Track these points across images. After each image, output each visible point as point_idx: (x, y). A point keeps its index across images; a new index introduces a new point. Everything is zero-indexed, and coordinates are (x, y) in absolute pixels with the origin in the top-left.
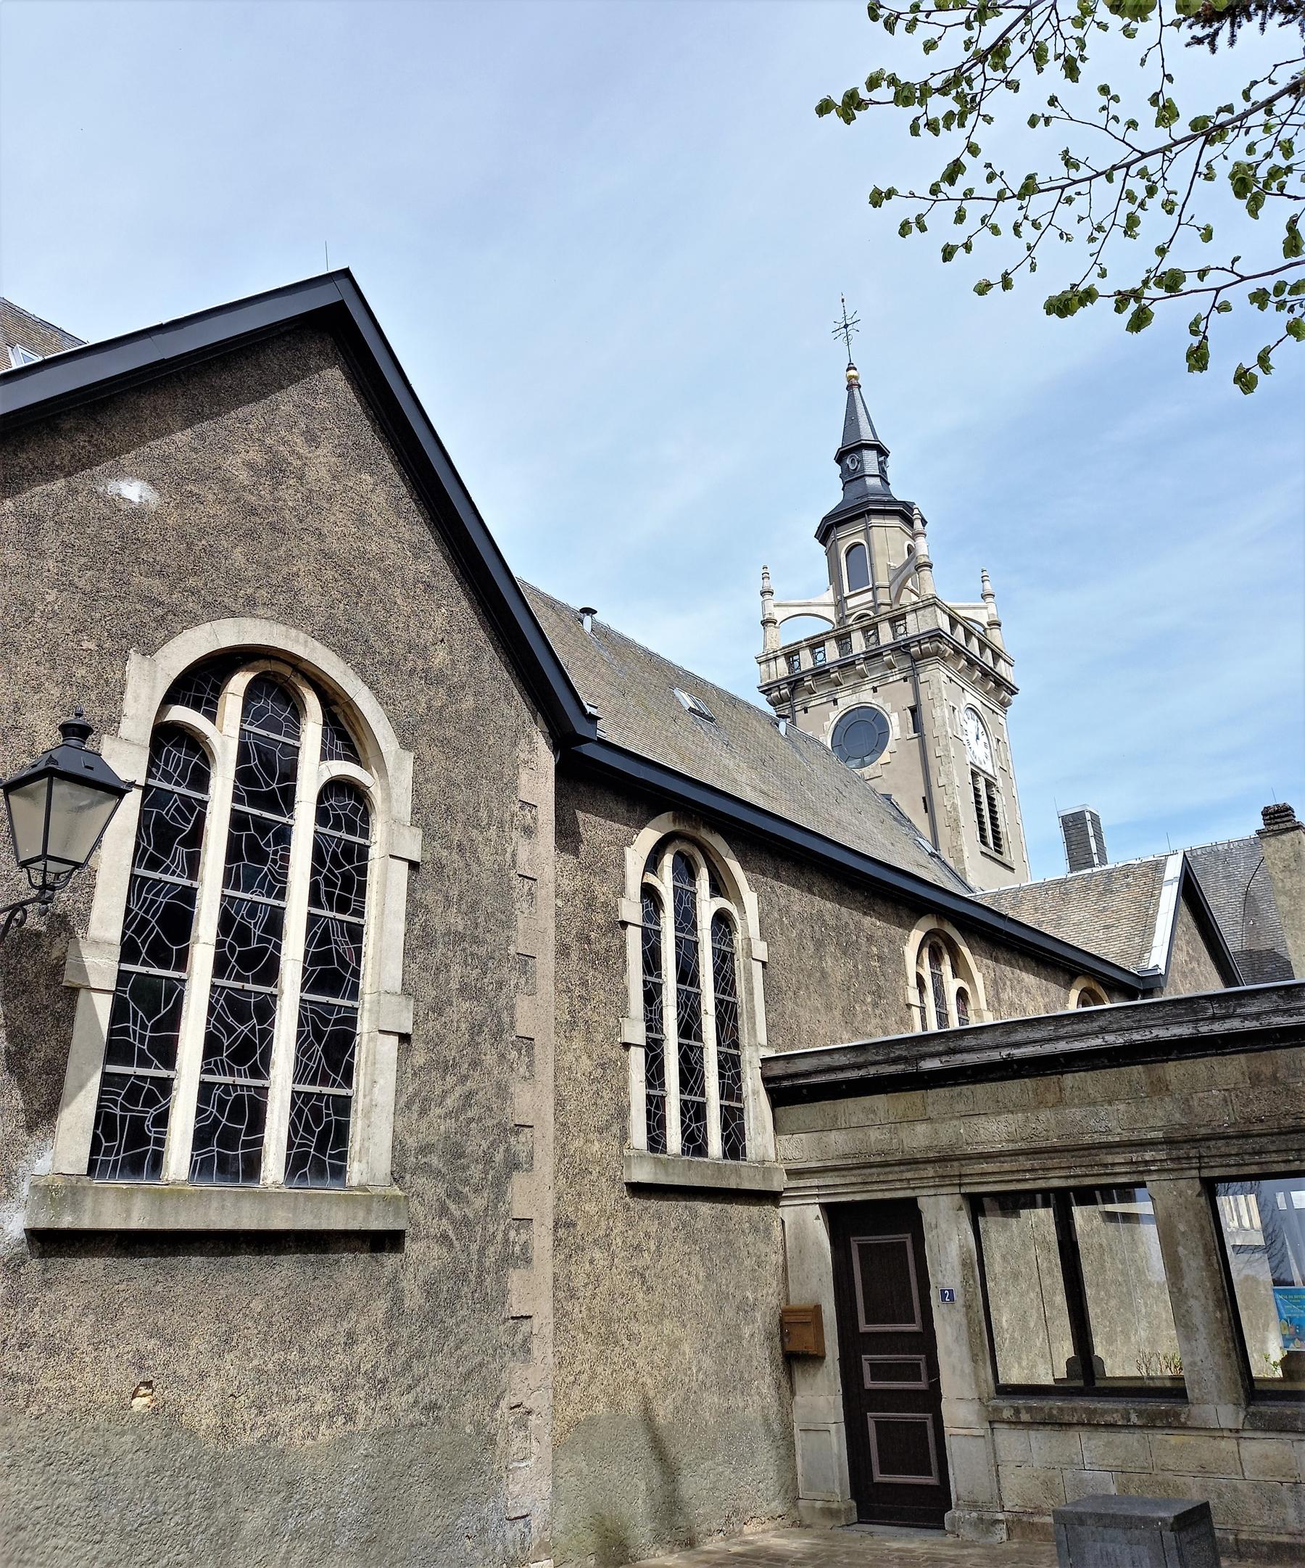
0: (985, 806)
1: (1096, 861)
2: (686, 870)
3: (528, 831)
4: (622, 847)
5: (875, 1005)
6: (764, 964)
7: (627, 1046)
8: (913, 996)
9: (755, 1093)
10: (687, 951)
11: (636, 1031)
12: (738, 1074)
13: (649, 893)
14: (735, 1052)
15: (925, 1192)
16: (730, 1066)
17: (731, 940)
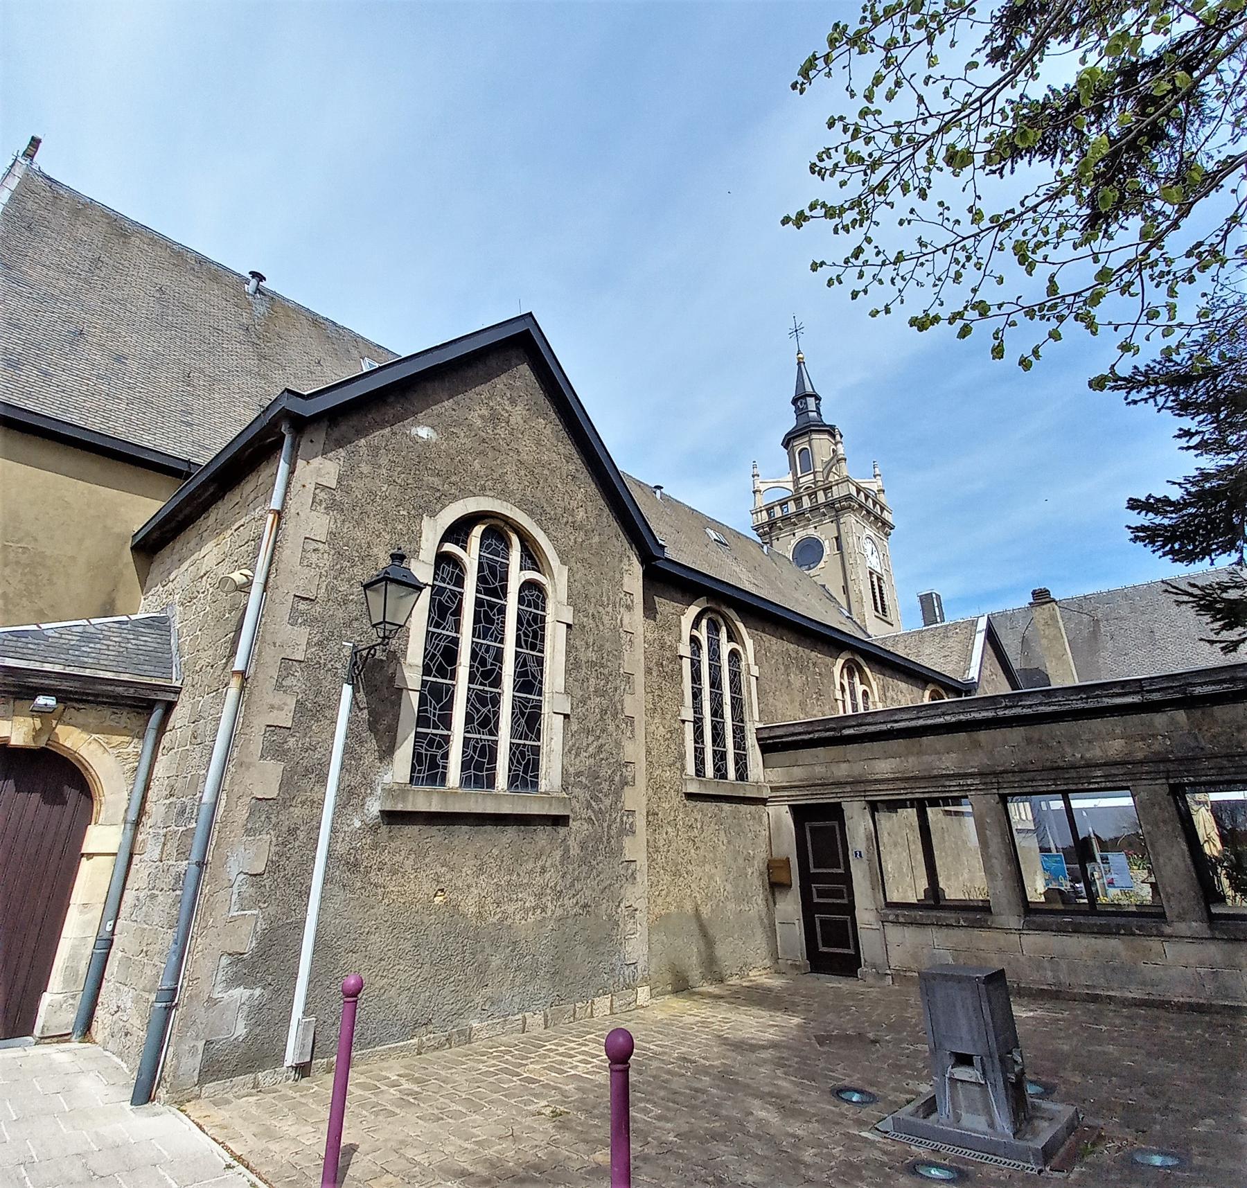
0: (877, 590)
7: (683, 721)
8: (838, 695)
11: (688, 714)
13: (694, 640)
16: (739, 731)
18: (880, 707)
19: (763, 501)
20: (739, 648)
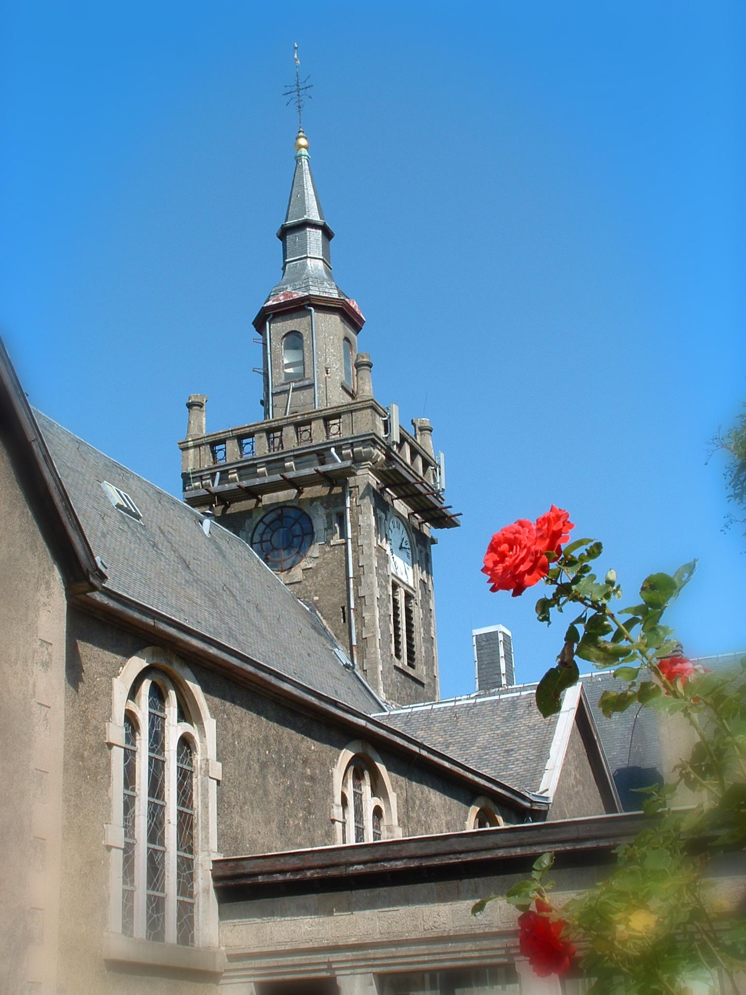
0: (403, 618)
1: (504, 681)
2: (158, 696)
3: (46, 665)
4: (111, 678)
5: (306, 820)
6: (218, 782)
7: (109, 848)
8: (337, 812)
9: (206, 891)
10: (157, 767)
11: (115, 835)
12: (191, 875)
13: (131, 719)
14: (189, 856)
15: (343, 972)
16: (186, 867)
17: (191, 760)
18: (399, 835)
19: (203, 425)
20: (193, 730)
